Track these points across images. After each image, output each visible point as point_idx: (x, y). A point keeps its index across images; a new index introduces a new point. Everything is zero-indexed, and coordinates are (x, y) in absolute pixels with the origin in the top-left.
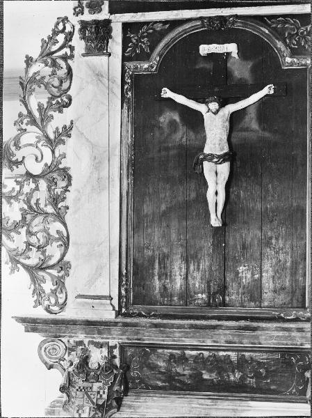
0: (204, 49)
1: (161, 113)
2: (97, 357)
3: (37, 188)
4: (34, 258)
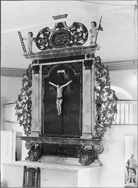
0: (59, 72)
1: (50, 87)
2: (36, 145)
3: (25, 106)
4: (25, 122)
